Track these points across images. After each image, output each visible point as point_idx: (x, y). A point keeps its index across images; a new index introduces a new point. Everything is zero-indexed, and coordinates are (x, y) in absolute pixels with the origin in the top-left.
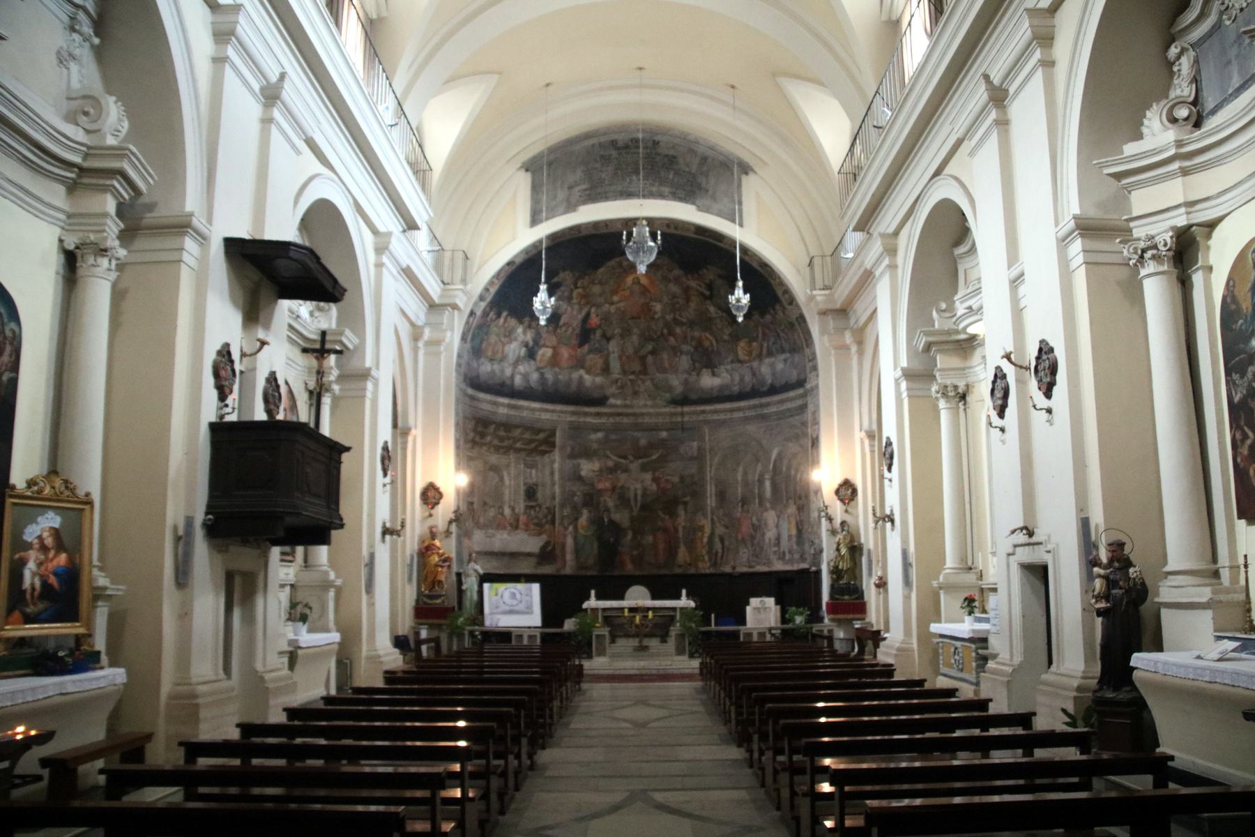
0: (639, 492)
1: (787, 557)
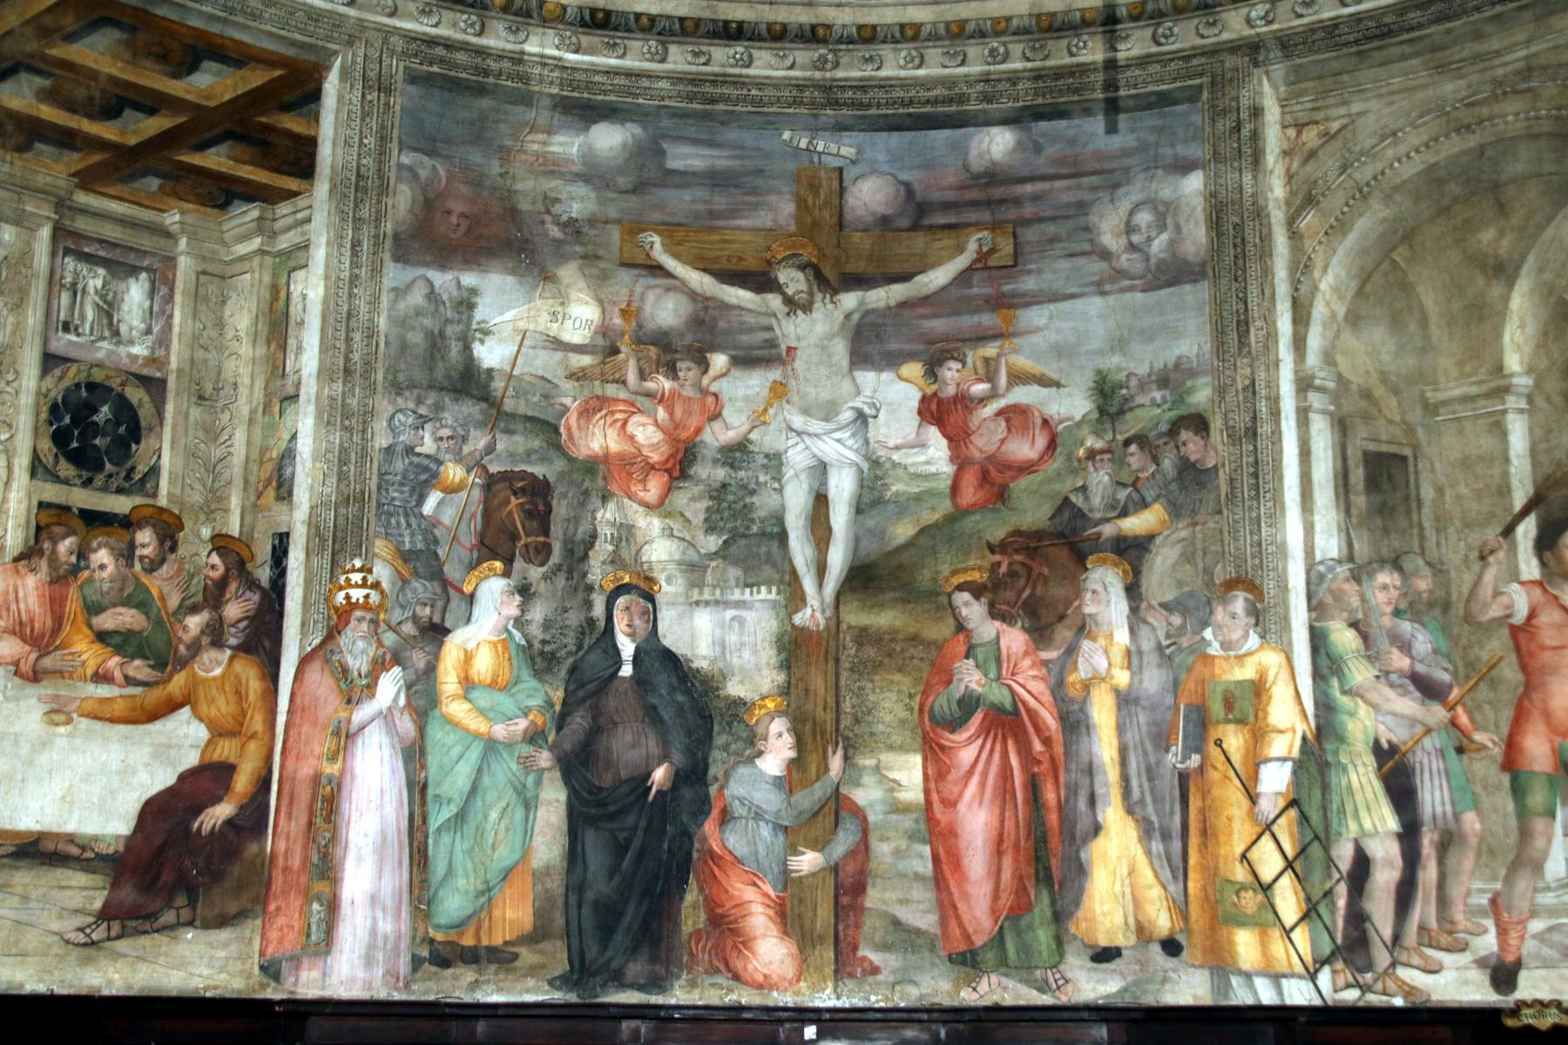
0: (842, 487)
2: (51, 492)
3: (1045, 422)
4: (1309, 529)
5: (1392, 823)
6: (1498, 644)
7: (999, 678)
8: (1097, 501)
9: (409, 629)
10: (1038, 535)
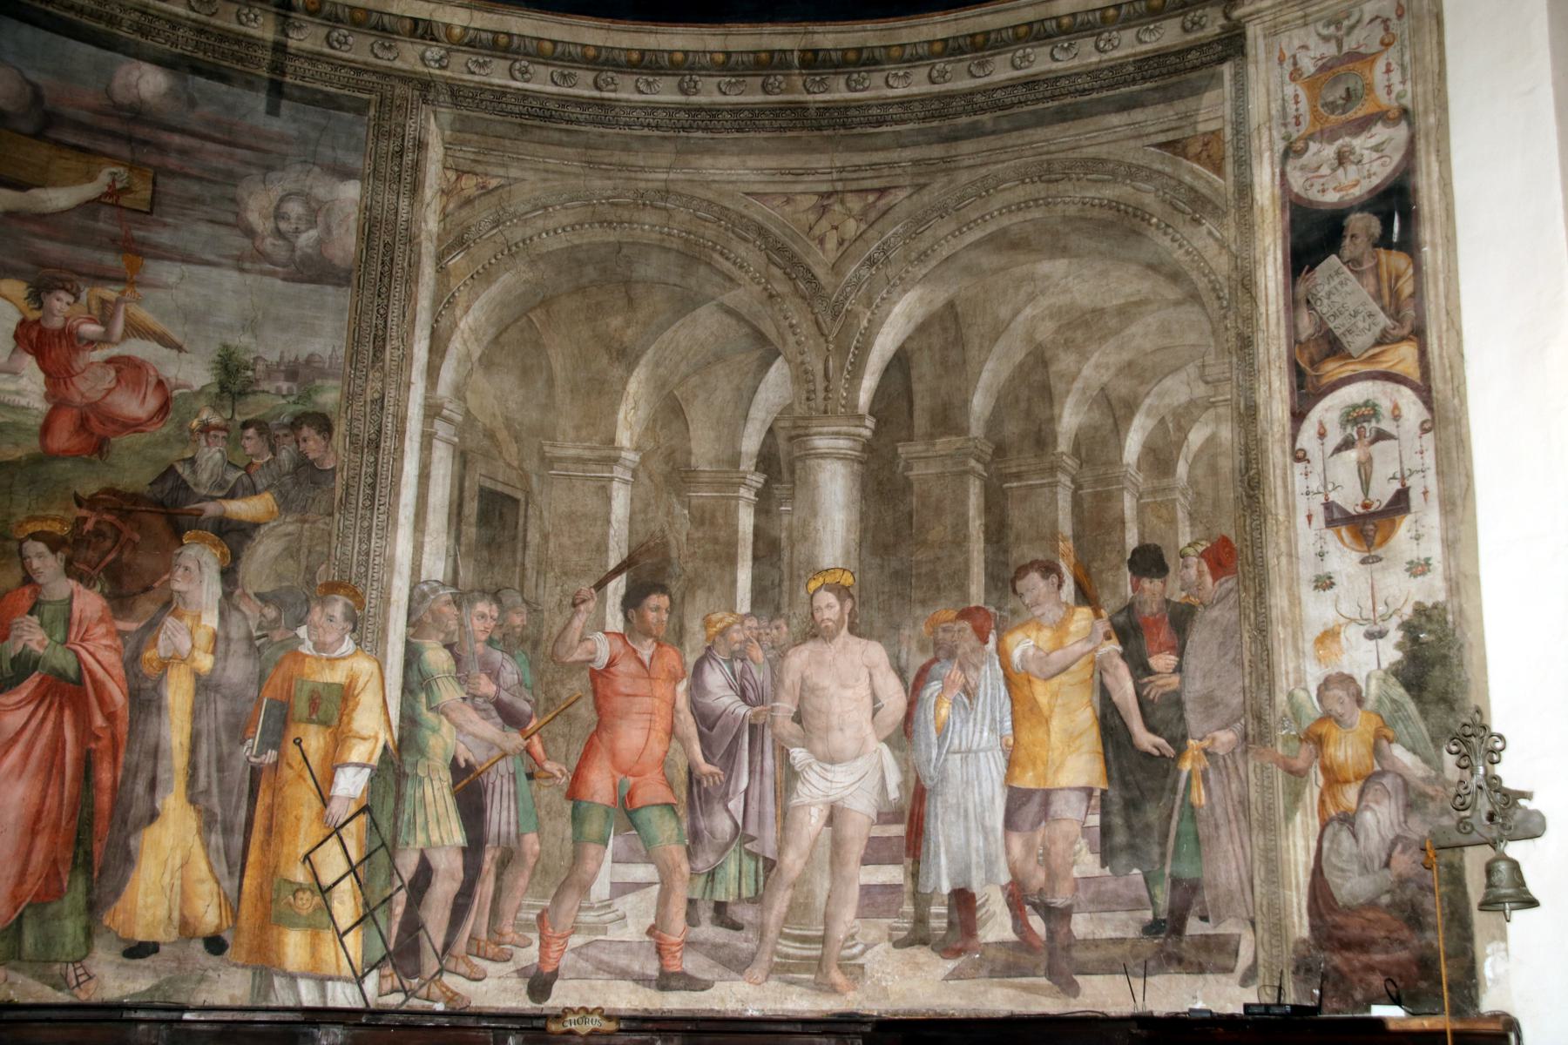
1: (997, 926)
3: (160, 384)
4: (418, 548)
5: (459, 838)
6: (578, 684)
7: (65, 641)
8: (204, 477)
10: (136, 498)
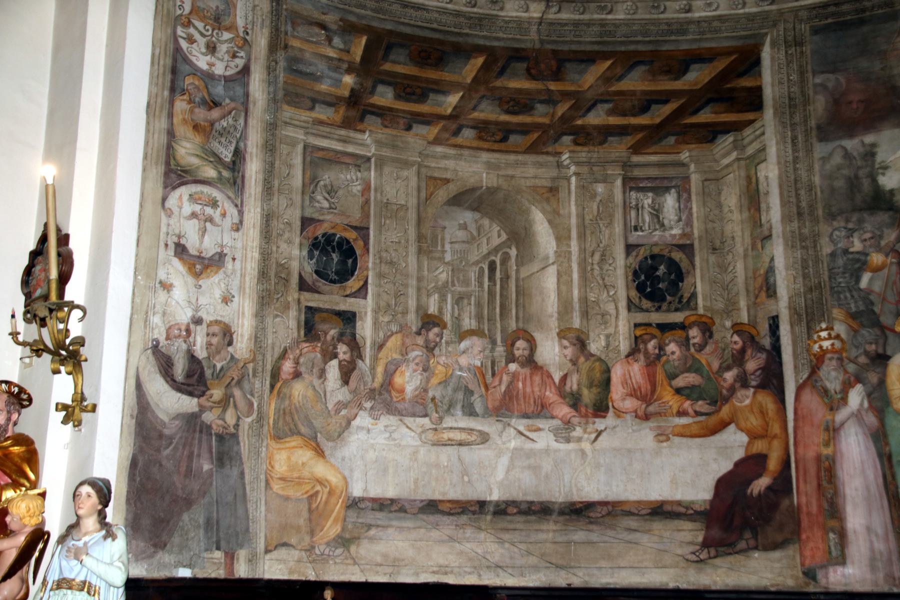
2: (640, 318)
9: (863, 360)
